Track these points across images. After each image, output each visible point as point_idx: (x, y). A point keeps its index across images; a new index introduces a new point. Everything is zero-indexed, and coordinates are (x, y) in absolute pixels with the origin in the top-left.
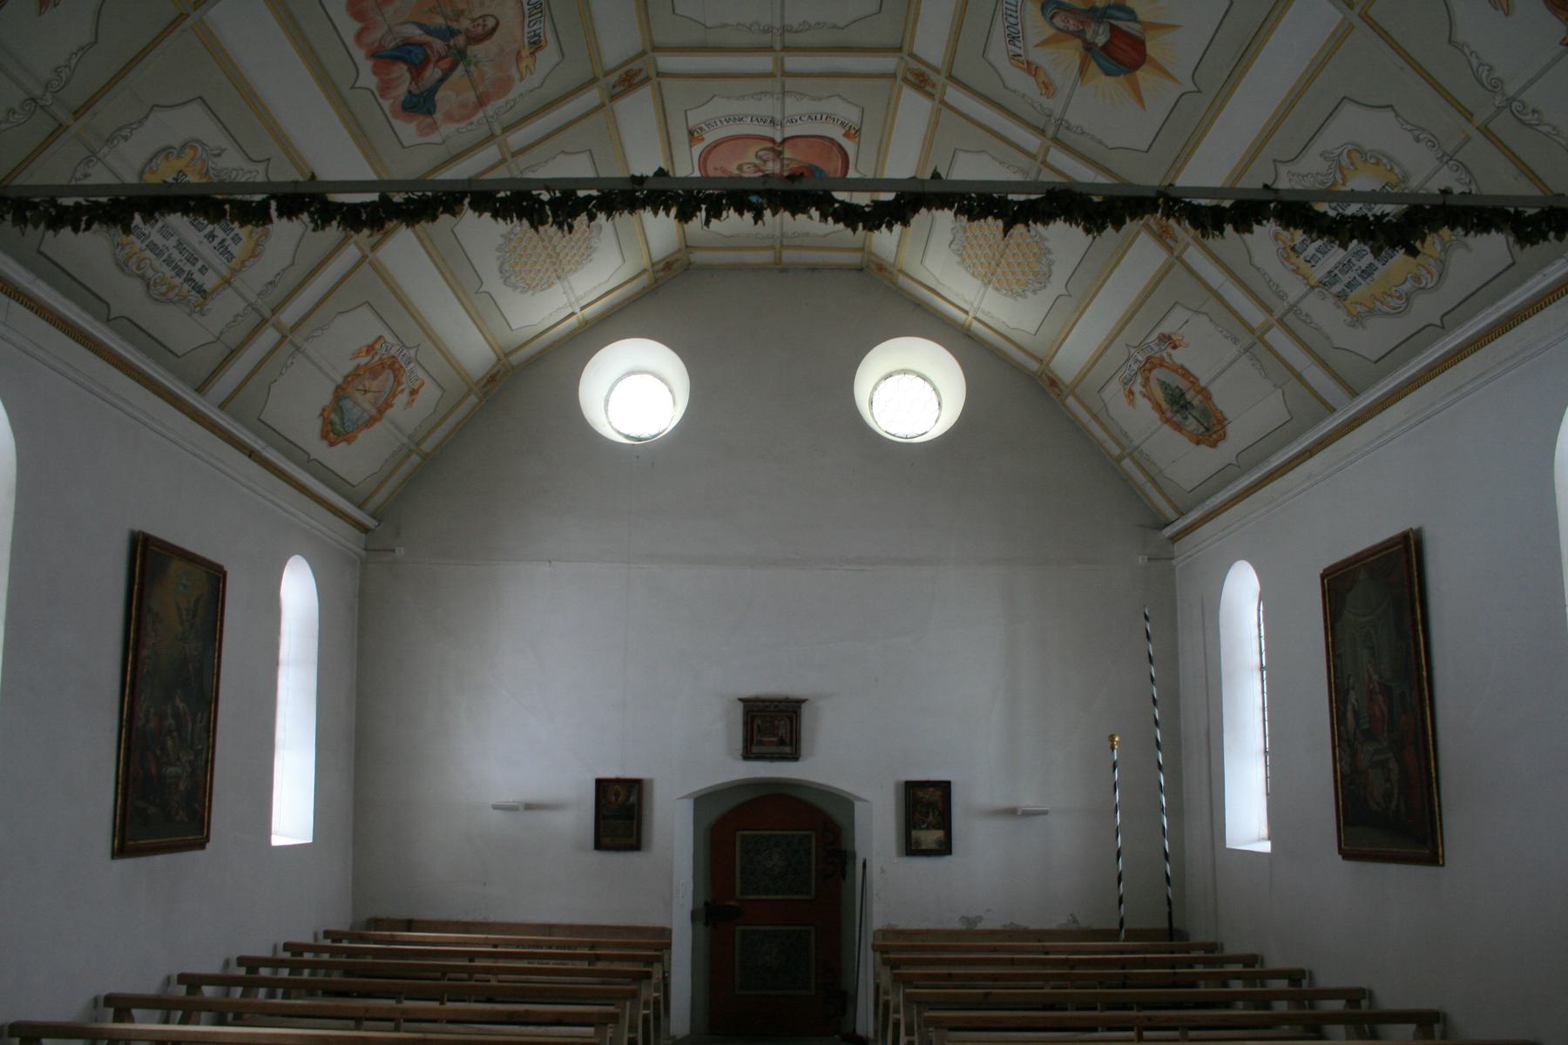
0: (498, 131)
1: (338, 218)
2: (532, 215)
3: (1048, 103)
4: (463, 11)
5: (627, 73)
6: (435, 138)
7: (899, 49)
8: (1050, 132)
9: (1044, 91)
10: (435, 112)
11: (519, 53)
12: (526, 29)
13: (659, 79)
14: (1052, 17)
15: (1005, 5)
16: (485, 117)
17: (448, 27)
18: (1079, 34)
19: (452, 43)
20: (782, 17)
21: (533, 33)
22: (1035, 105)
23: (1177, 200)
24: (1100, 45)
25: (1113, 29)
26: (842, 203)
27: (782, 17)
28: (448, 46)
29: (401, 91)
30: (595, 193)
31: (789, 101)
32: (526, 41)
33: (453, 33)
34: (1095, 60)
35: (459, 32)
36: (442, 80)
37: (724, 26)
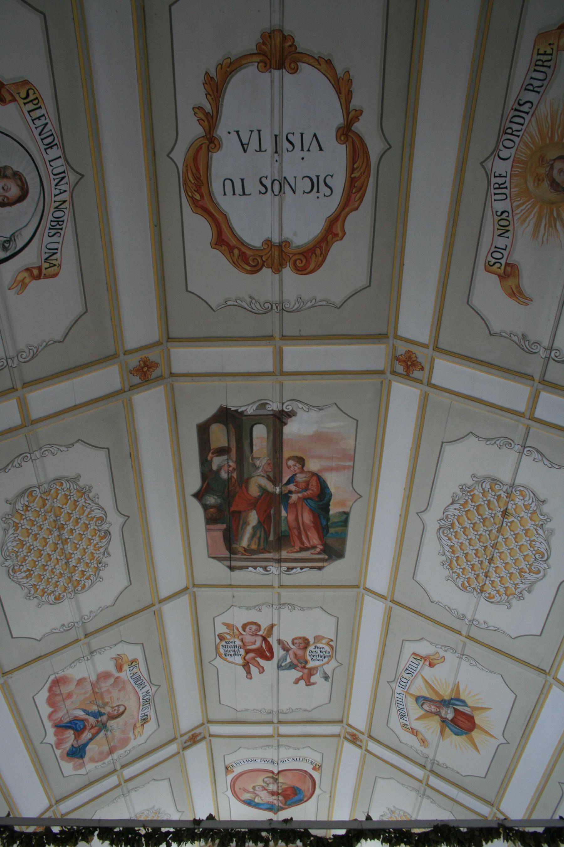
0: (118, 767)
1: (18, 842)
2: (133, 844)
3: (426, 751)
4: (108, 703)
5: (193, 735)
6: (83, 771)
7: (341, 722)
8: (429, 767)
9: (422, 744)
10: (84, 757)
11: (135, 725)
12: (141, 712)
13: (210, 738)
14: (422, 705)
15: (396, 699)
16: (113, 760)
17: (99, 711)
18: (438, 714)
19: (100, 719)
20: (278, 705)
21: (144, 715)
22: (418, 752)
23: (511, 829)
24: (450, 719)
25: (455, 710)
26: (315, 837)
27: (278, 705)
28: (98, 721)
29: (67, 746)
30: (172, 830)
31: (282, 750)
32: (140, 718)
33: (101, 714)
34: (448, 727)
35: (105, 714)
36: (91, 739)
37: (247, 710)
